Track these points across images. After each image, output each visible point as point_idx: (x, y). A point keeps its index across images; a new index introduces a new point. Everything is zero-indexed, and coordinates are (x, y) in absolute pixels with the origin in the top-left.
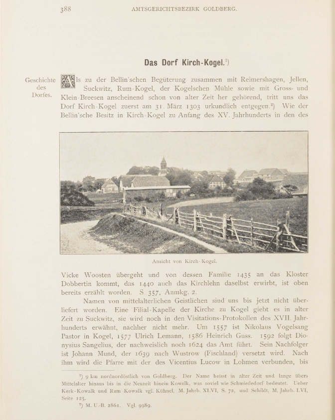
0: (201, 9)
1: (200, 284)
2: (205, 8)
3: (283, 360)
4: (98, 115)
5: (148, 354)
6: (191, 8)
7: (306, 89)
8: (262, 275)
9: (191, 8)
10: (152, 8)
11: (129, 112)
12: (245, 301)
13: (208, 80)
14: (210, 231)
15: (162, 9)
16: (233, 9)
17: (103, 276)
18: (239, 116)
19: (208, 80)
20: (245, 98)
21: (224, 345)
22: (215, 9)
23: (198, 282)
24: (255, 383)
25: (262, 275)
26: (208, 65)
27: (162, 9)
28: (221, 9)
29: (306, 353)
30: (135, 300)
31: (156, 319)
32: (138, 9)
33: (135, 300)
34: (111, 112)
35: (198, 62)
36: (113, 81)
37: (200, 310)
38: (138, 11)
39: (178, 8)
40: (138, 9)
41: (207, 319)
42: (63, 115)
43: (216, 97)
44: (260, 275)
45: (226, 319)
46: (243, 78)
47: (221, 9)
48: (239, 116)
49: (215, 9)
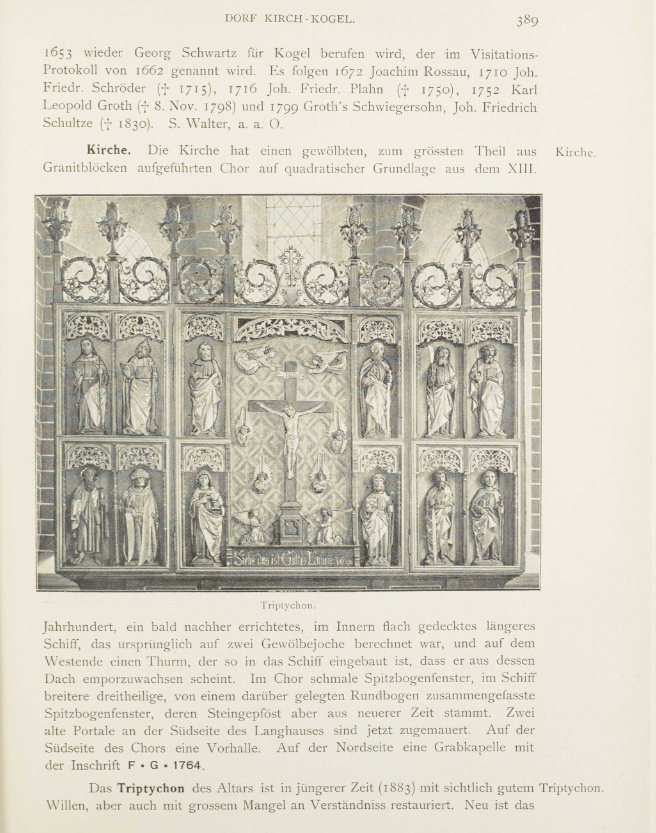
0: (260, 18)
1: (198, 151)
2: (139, 51)
3: (128, 84)
4: (167, 56)
13: (468, 714)
14: (421, 350)
18: (55, 628)
19: (468, 714)
21: (497, 731)
23: (194, 148)
24: (110, 88)
26: (94, 153)
29: (50, 661)
35: (298, 18)
37: (189, 152)
41: (330, 170)
43: (167, 731)
45: (49, 71)
48: (55, 628)
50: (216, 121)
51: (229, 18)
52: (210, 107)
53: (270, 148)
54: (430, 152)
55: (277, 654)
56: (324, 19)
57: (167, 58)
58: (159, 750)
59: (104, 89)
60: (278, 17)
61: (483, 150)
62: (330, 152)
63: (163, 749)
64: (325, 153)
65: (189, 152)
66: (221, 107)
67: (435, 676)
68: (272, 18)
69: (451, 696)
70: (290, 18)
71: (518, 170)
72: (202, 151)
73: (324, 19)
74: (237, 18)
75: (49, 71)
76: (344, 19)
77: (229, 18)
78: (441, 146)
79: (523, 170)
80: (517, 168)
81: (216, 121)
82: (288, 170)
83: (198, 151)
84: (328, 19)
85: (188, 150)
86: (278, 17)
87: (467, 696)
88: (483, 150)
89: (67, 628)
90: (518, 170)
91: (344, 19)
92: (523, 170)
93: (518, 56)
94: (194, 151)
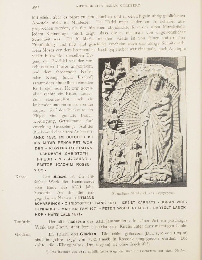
1: (125, 227)
2: (121, 5)
5: (74, 240)
6: (112, 5)
7: (171, 233)
8: (83, 176)
9: (112, 5)
10: (88, 6)
11: (82, 70)
12: (74, 50)
15: (94, 6)
16: (139, 5)
17: (86, 23)
20: (40, 40)
22: (127, 6)
23: (124, 226)
24: (38, 40)
25: (83, 176)
27: (94, 6)
28: (131, 6)
30: (74, 226)
31: (76, 245)
32: (80, 6)
33: (74, 226)
34: (92, 37)
36: (98, 50)
38: (80, 8)
39: (104, 6)
40: (80, 6)
42: (37, 245)
44: (73, 67)
46: (69, 109)
47: (131, 6)
49: (127, 6)
50: (67, 131)
53: (164, 220)
54: (130, 234)
55: (58, 53)
57: (73, 128)
59: (36, 40)
61: (59, 234)
62: (169, 33)
64: (178, 44)
67: (44, 17)
69: (77, 121)
71: (99, 222)
72: (127, 227)
78: (88, 4)
80: (98, 221)
81: (67, 131)
82: (110, 227)
83: (125, 227)
88: (59, 234)
90: (99, 222)
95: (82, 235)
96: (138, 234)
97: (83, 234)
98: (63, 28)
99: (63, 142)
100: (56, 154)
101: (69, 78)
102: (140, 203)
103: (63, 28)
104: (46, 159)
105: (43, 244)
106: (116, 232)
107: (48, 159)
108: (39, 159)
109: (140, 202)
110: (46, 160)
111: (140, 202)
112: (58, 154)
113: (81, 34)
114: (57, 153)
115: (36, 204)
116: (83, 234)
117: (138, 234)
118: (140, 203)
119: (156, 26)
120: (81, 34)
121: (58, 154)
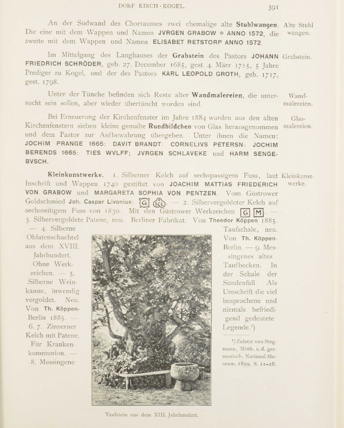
13: (45, 354)
23: (33, 124)
51: (121, 6)
52: (46, 82)
56: (169, 6)
58: (243, 57)
60: (145, 5)
63: (245, 57)
65: (118, 118)
66: (51, 82)
68: (143, 6)
70: (152, 6)
73: (169, 6)
74: (125, 6)
75: (28, 73)
76: (180, 6)
77: (121, 6)
79: (160, 415)
80: (158, 415)
83: (123, 118)
84: (171, 6)
85: (30, 125)
86: (145, 5)
87: (43, 354)
89: (46, 256)
91: (180, 6)
92: (160, 415)
93: (58, 354)
94: (121, 118)
95: (175, 56)
96: (299, 104)
97: (177, 56)
98: (222, 118)
99: (43, 152)
100: (214, 184)
101: (39, 336)
102: (166, 74)
103: (222, 118)
104: (40, 63)
105: (67, 334)
106: (94, 44)
107: (43, 63)
108: (29, 63)
109: (166, 73)
110: (41, 64)
111: (166, 73)
112: (233, 74)
113: (67, 256)
114: (220, 183)
115: (27, 152)
116: (177, 56)
117: (299, 104)
118: (166, 74)
119: (183, 94)
120: (67, 256)
121: (233, 74)
